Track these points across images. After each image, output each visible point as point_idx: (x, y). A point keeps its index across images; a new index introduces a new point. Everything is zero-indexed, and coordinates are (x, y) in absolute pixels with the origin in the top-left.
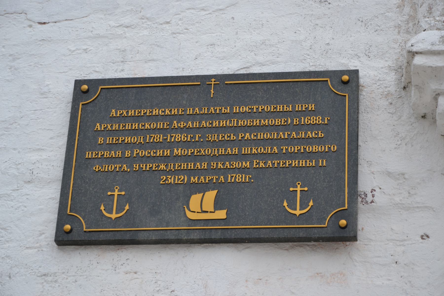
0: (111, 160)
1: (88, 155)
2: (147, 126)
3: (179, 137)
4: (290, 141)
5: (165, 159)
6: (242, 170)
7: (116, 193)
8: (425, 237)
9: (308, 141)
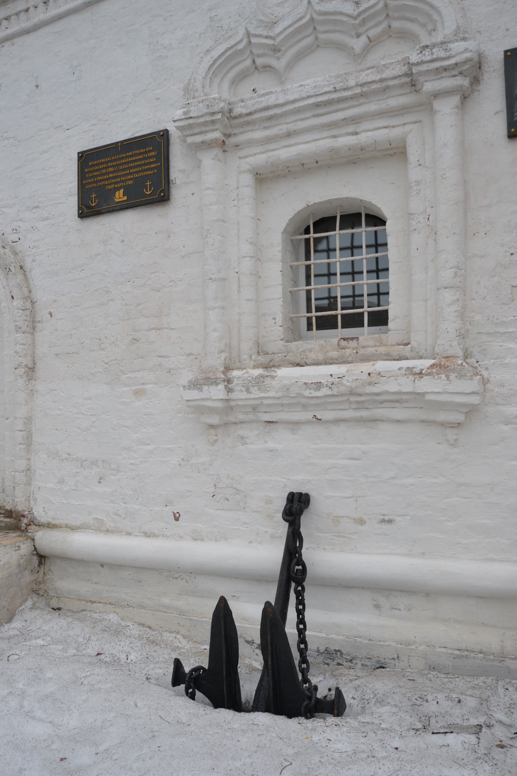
0: (91, 183)
1: (84, 182)
2: (101, 167)
3: (111, 169)
4: (145, 164)
5: (107, 179)
6: (131, 179)
7: (148, 183)
8: (193, 194)
9: (151, 163)
